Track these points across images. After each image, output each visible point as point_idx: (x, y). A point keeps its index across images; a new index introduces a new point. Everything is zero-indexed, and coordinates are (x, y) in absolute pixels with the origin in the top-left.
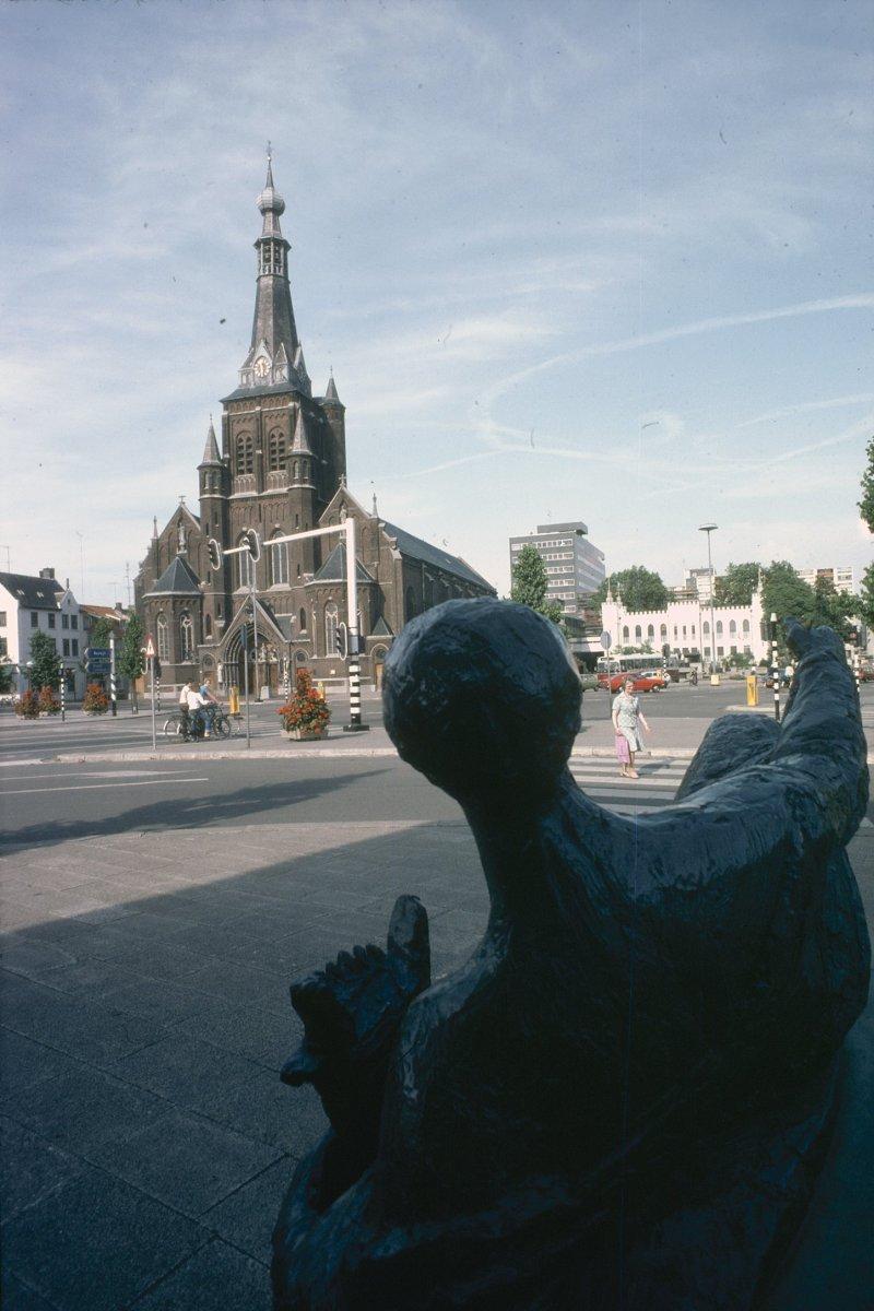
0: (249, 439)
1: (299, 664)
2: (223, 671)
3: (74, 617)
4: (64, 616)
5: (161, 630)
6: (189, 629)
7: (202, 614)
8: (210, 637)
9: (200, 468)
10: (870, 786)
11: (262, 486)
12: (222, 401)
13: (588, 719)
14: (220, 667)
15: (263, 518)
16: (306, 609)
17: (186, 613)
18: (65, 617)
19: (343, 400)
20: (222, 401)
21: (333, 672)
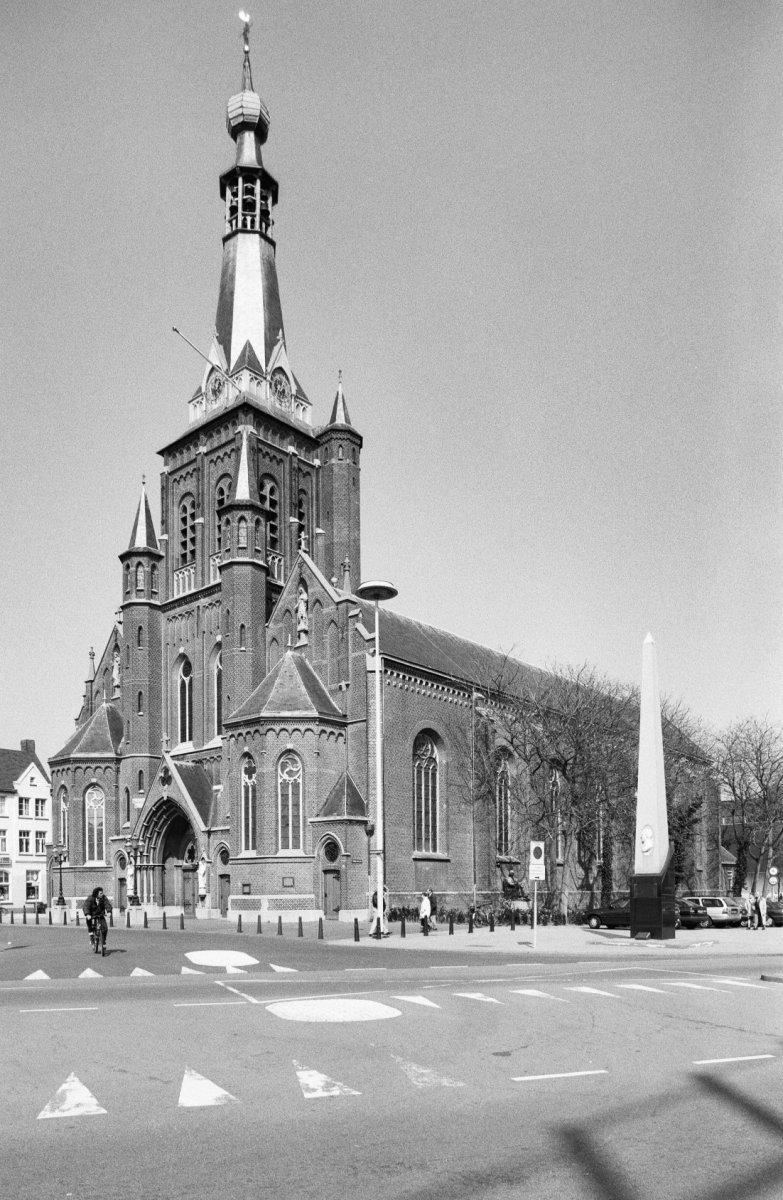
3: (40, 802)
6: (296, 785)
8: (128, 824)
12: (161, 453)
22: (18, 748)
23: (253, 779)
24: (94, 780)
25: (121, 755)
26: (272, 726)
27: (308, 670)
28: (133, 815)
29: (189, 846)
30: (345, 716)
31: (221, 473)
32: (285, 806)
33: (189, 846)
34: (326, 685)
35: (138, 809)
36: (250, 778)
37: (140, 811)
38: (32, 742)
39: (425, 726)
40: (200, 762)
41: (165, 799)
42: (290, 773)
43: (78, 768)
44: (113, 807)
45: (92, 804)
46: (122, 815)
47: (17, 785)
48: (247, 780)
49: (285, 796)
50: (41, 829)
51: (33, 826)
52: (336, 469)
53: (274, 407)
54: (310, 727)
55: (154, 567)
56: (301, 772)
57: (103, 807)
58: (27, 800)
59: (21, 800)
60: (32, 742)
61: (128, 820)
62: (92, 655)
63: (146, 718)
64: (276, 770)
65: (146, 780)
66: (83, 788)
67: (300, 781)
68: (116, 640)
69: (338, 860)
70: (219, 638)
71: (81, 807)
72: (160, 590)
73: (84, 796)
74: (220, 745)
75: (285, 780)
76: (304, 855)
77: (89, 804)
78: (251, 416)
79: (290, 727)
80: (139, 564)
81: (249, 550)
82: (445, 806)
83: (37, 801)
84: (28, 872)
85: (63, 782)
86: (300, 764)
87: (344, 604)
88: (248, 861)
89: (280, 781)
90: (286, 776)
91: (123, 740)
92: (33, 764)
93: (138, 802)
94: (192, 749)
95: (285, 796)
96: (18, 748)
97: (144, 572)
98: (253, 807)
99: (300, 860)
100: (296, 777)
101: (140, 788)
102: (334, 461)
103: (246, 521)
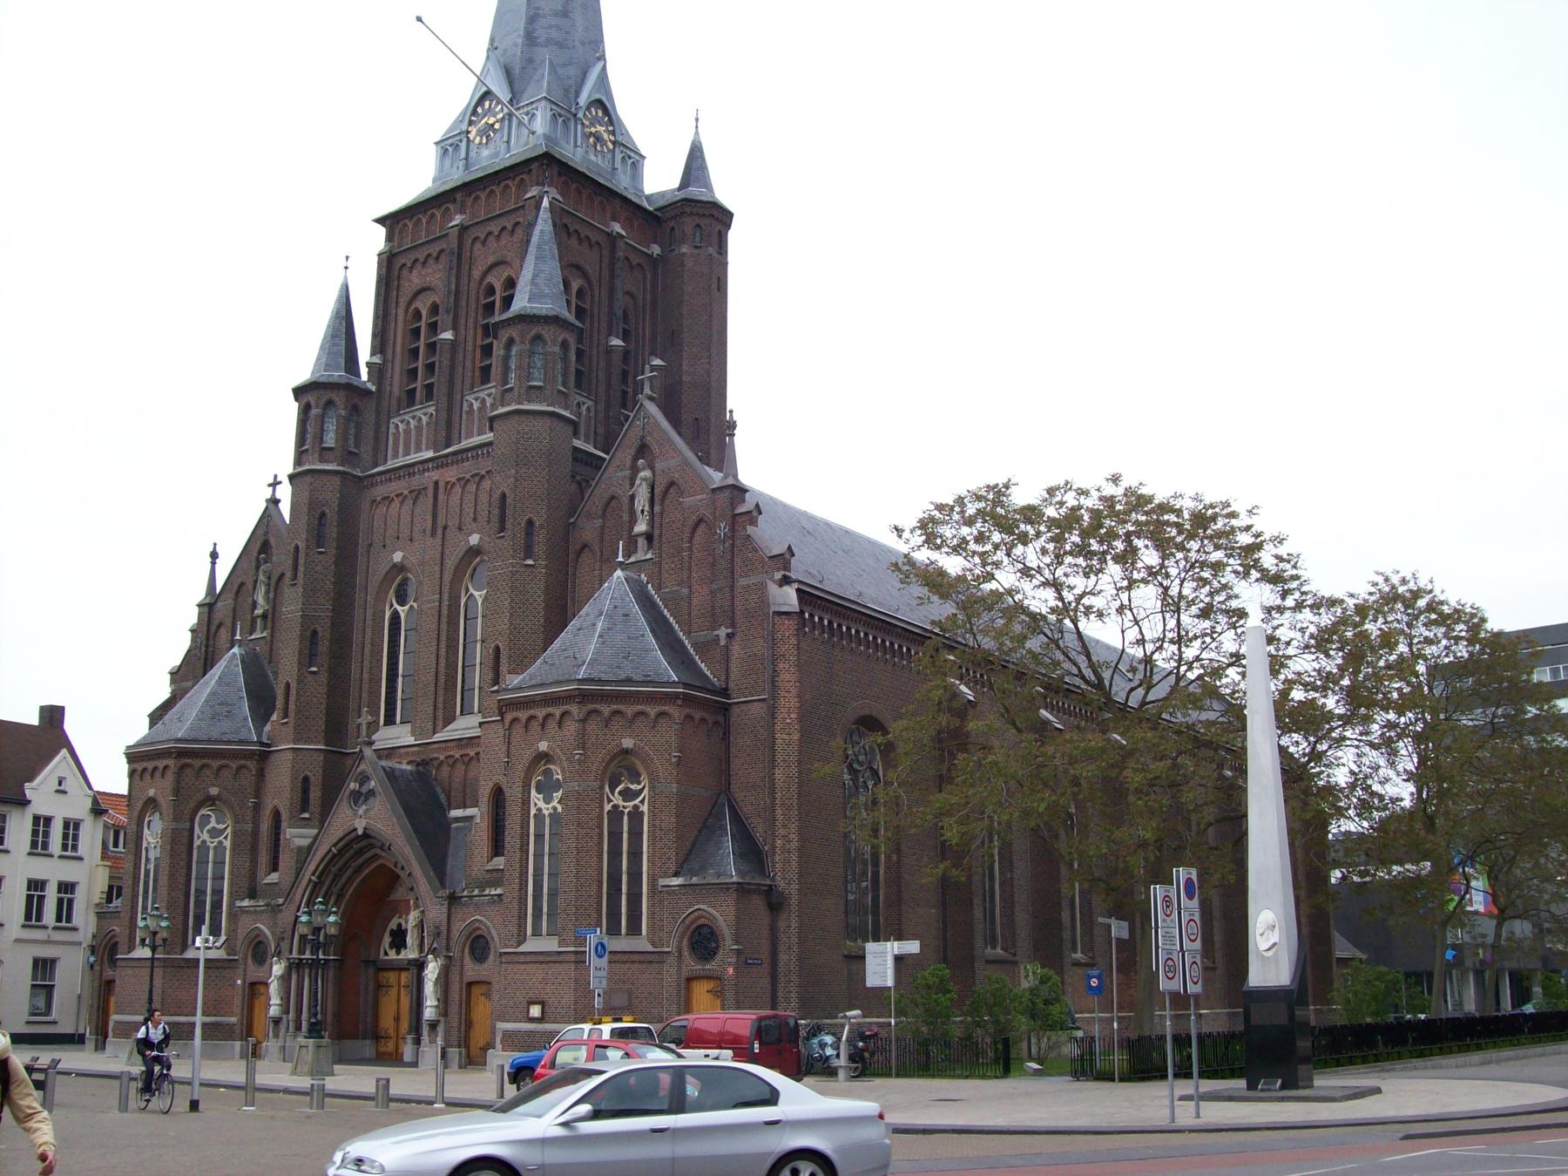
0: (434, 309)
1: (472, 970)
2: (285, 979)
3: (71, 826)
4: (36, 819)
5: (539, 816)
6: (636, 815)
7: (257, 808)
8: (274, 877)
9: (299, 392)
10: (1508, 630)
11: (447, 429)
12: (381, 221)
13: (1498, 1003)
14: (278, 969)
15: (441, 521)
16: (513, 793)
17: (210, 801)
18: (42, 824)
19: (724, 191)
20: (381, 221)
21: (535, 1011)
22: (33, 719)
23: (555, 803)
24: (214, 791)
25: (269, 745)
26: (597, 706)
27: (654, 605)
28: (286, 860)
29: (393, 925)
30: (725, 692)
31: (491, 259)
32: (615, 854)
33: (393, 925)
34: (688, 633)
35: (300, 849)
36: (548, 800)
37: (304, 854)
38: (61, 710)
39: (867, 712)
40: (424, 763)
41: (360, 832)
42: (628, 795)
43: (226, 766)
44: (247, 844)
45: (205, 836)
46: (264, 859)
47: (30, 790)
48: (541, 804)
49: (615, 837)
50: (68, 878)
51: (53, 871)
52: (689, 264)
53: (585, 159)
54: (666, 708)
55: (355, 409)
56: (646, 791)
57: (227, 844)
58: (48, 820)
59: (36, 819)
60: (61, 710)
61: (275, 869)
62: (214, 556)
63: (324, 678)
64: (602, 788)
65: (315, 794)
66: (192, 804)
67: (645, 808)
68: (266, 533)
69: (718, 958)
70: (474, 539)
71: (185, 840)
72: (366, 450)
73: (192, 821)
74: (477, 732)
75: (615, 807)
76: (650, 949)
77: (202, 836)
78: (556, 170)
79: (630, 710)
80: (330, 403)
81: (548, 393)
82: (895, 857)
83: (66, 824)
84: (36, 961)
85: (151, 793)
86: (645, 781)
87: (727, 493)
88: (541, 958)
89: (608, 807)
90: (617, 800)
91: (274, 717)
92: (64, 752)
93: (297, 836)
94: (411, 740)
95: (615, 837)
96: (33, 719)
97: (339, 416)
98: (993, 922)
99: (641, 958)
100: (637, 802)
101: (304, 810)
102: (685, 249)
103: (545, 343)
